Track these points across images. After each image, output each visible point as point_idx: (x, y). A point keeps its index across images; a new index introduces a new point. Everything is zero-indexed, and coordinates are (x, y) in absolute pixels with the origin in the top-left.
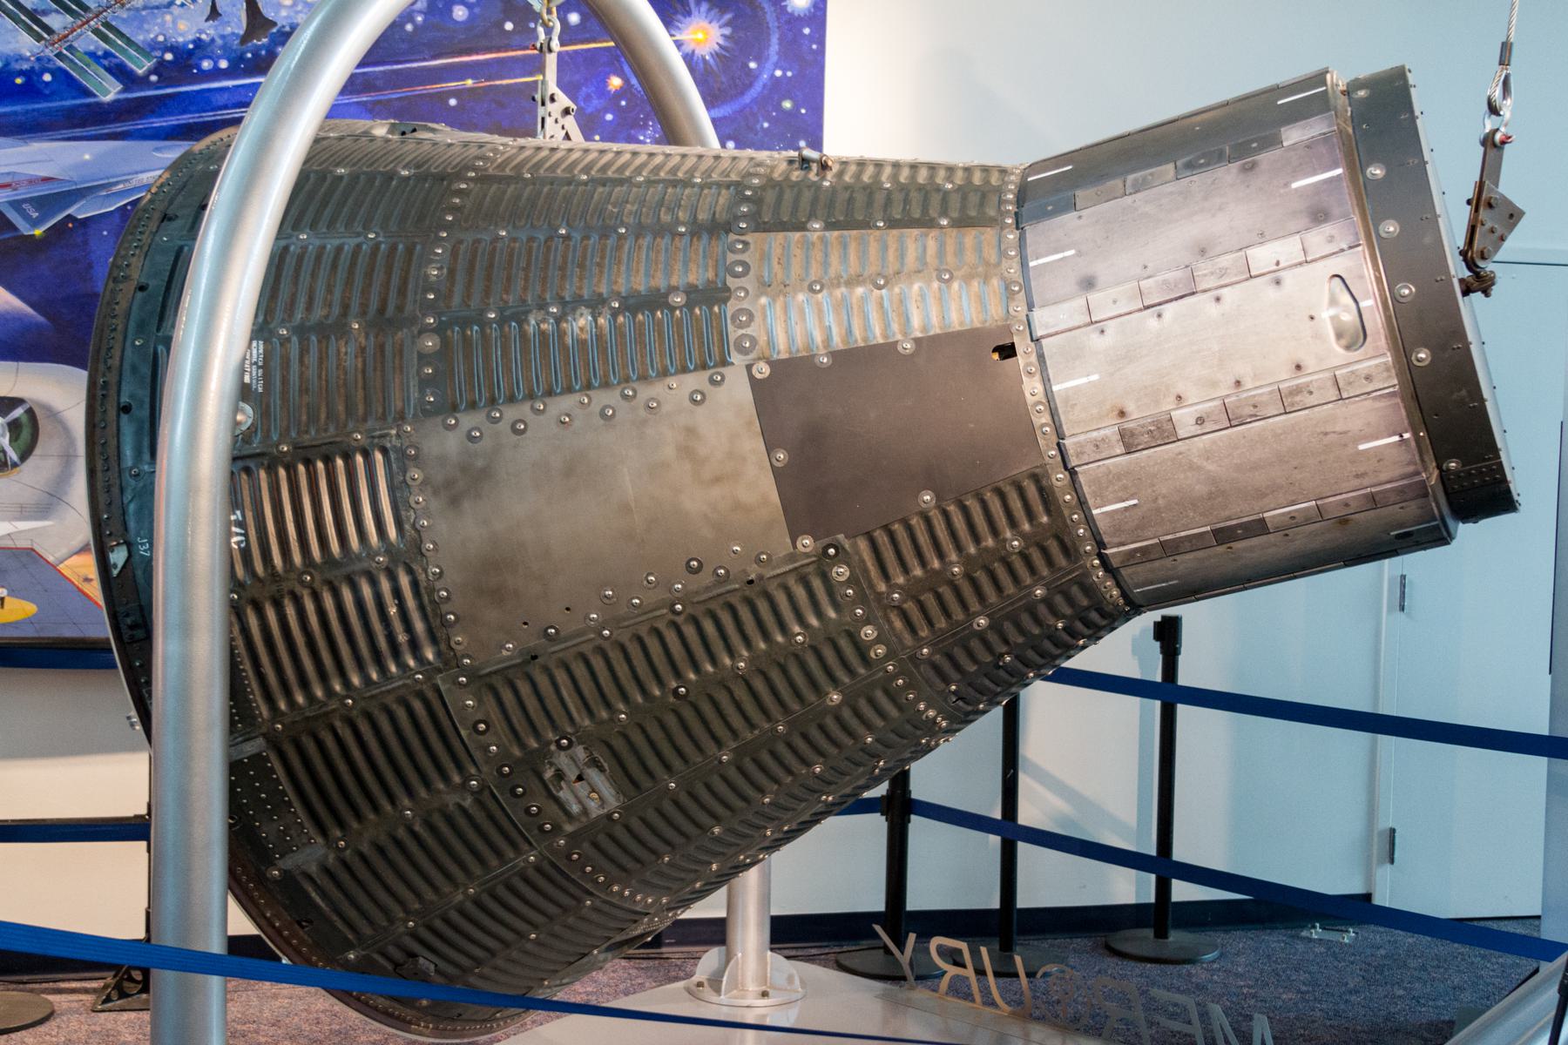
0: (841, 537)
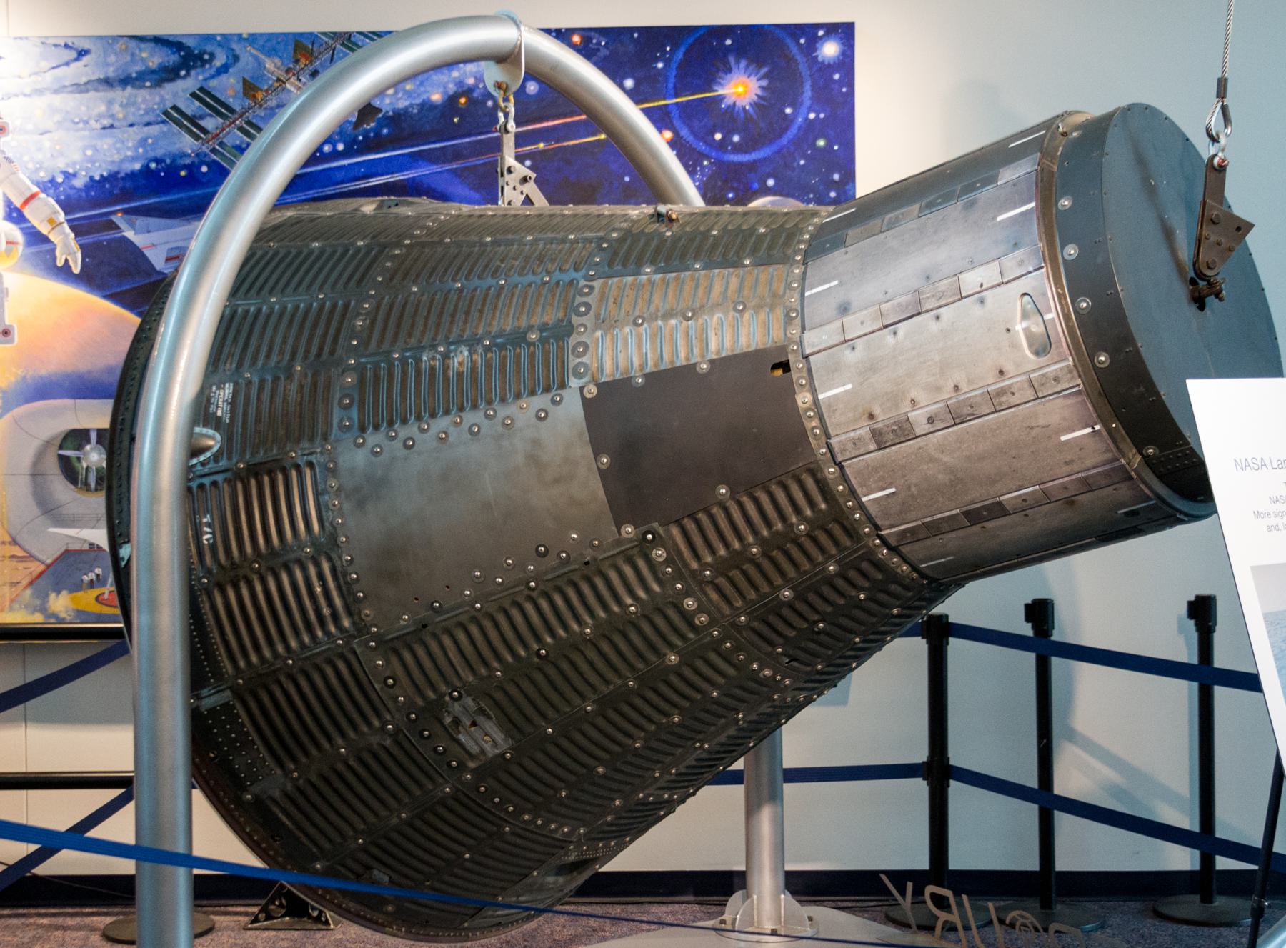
0: (656, 525)
